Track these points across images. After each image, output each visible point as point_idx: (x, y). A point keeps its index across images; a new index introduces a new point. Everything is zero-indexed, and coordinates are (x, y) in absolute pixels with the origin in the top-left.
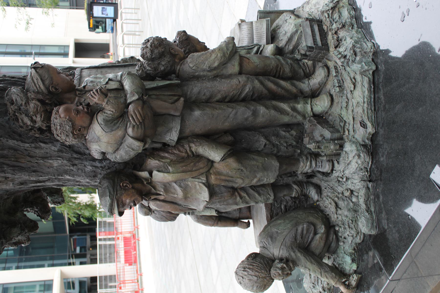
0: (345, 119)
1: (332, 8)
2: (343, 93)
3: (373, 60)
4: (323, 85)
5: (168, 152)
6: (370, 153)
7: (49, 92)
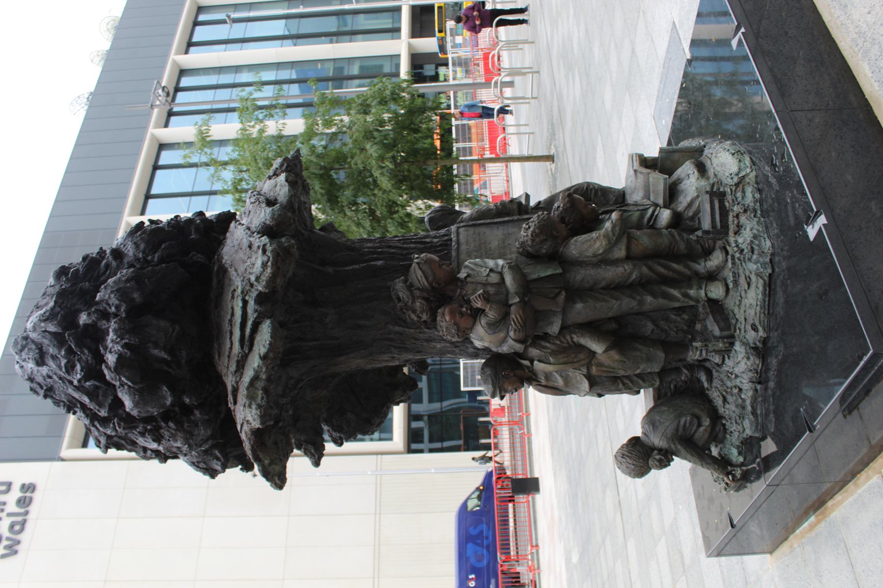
0: (737, 317)
1: (736, 184)
2: (737, 289)
3: (771, 260)
4: (721, 268)
5: (549, 342)
6: (761, 355)
7: (433, 288)
